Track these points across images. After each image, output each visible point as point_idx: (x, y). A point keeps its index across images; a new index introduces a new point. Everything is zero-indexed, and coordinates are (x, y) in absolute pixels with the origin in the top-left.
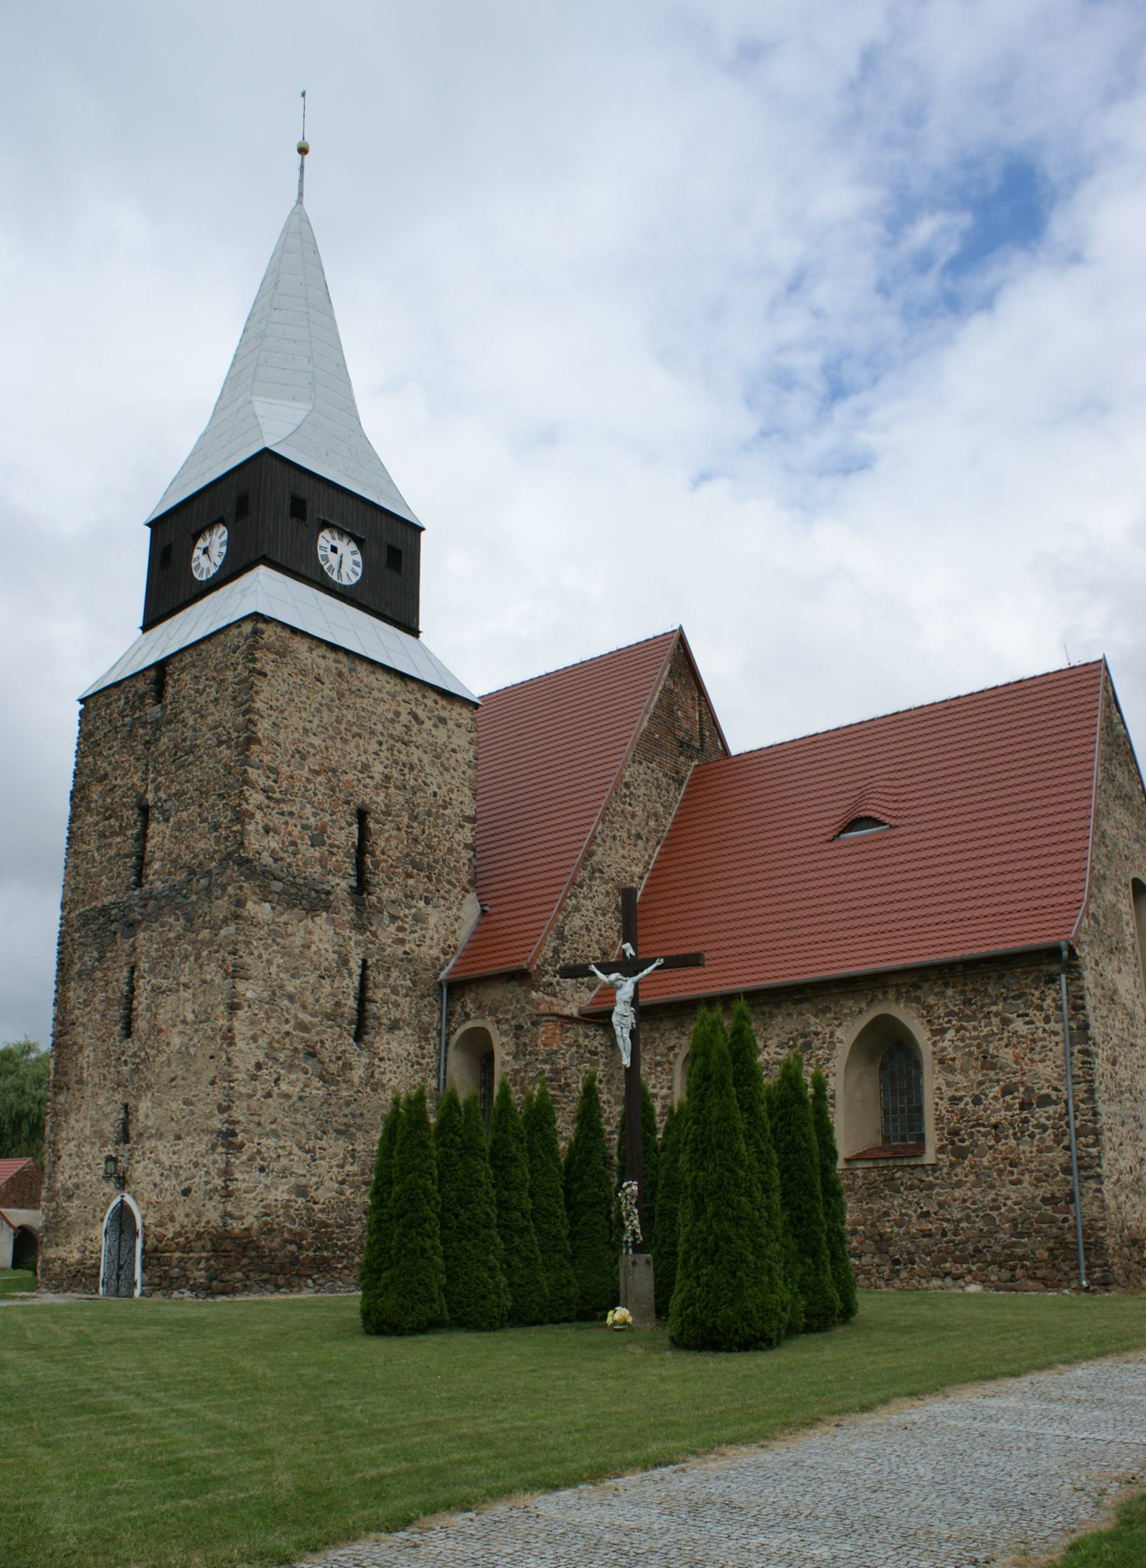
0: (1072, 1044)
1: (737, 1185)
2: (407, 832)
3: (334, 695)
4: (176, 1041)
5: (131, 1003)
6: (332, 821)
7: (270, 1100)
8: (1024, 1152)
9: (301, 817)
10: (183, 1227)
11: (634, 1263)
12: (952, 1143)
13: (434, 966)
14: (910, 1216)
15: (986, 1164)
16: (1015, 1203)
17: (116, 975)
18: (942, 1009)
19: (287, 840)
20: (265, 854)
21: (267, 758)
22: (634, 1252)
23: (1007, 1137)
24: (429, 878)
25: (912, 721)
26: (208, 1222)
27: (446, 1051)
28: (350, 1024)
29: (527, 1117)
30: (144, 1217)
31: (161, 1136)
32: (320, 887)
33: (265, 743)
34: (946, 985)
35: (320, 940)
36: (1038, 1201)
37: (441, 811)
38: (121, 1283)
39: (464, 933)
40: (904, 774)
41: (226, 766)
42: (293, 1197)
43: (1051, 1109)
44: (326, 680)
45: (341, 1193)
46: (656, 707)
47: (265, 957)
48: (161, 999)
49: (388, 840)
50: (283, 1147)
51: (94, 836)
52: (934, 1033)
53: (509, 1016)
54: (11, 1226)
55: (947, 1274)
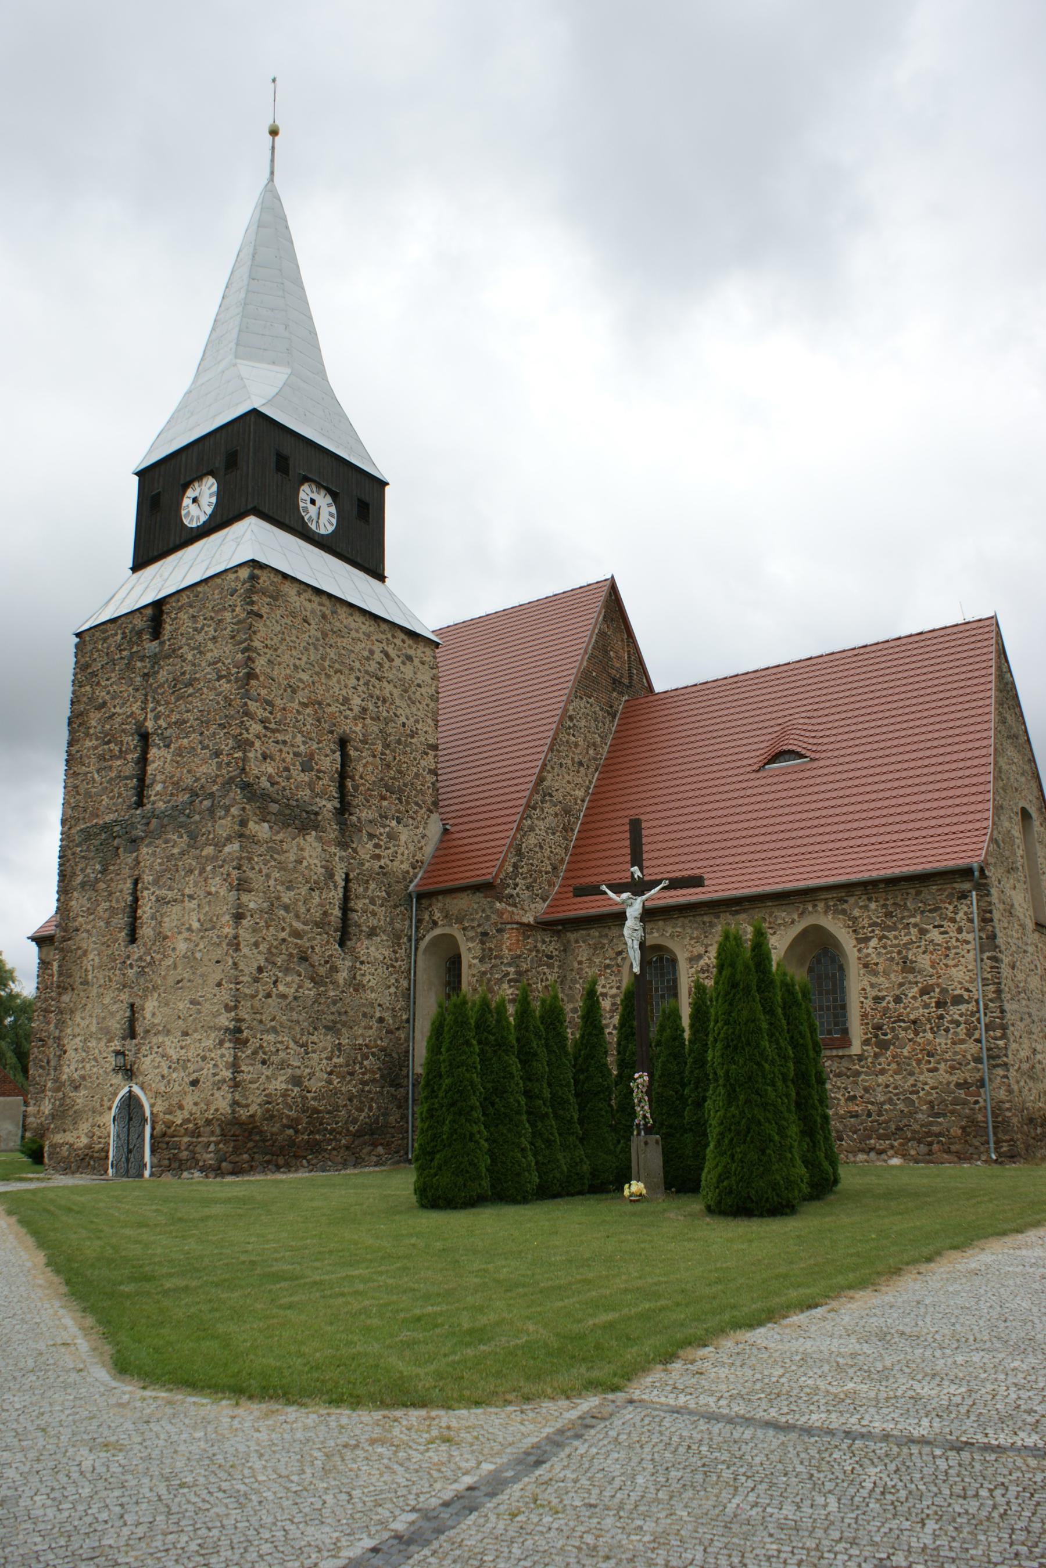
0: (982, 952)
1: (764, 1077)
3: (319, 635)
4: (182, 947)
5: (135, 912)
6: (319, 749)
7: (270, 1000)
8: (940, 1044)
9: (293, 746)
10: (191, 1114)
11: (646, 1143)
12: (876, 1036)
13: (404, 878)
14: (839, 1100)
15: (906, 1054)
16: (932, 1088)
17: (120, 887)
18: (866, 921)
19: (282, 766)
20: (264, 779)
21: (263, 692)
22: (646, 1134)
23: (925, 1031)
25: (825, 666)
26: (217, 1110)
27: (416, 955)
28: (336, 931)
29: (542, 1017)
30: (152, 1106)
31: (168, 1032)
33: (262, 679)
34: (870, 899)
35: (311, 856)
36: (952, 1086)
37: (409, 740)
38: (130, 1165)
39: (429, 850)
40: (820, 713)
41: (226, 698)
42: (290, 1087)
43: (963, 1007)
44: (312, 622)
45: (330, 1082)
46: (593, 648)
47: (265, 871)
48: (165, 909)
49: (365, 766)
50: (282, 1042)
51: (94, 760)
52: (859, 941)
53: (475, 924)
55: (872, 1149)
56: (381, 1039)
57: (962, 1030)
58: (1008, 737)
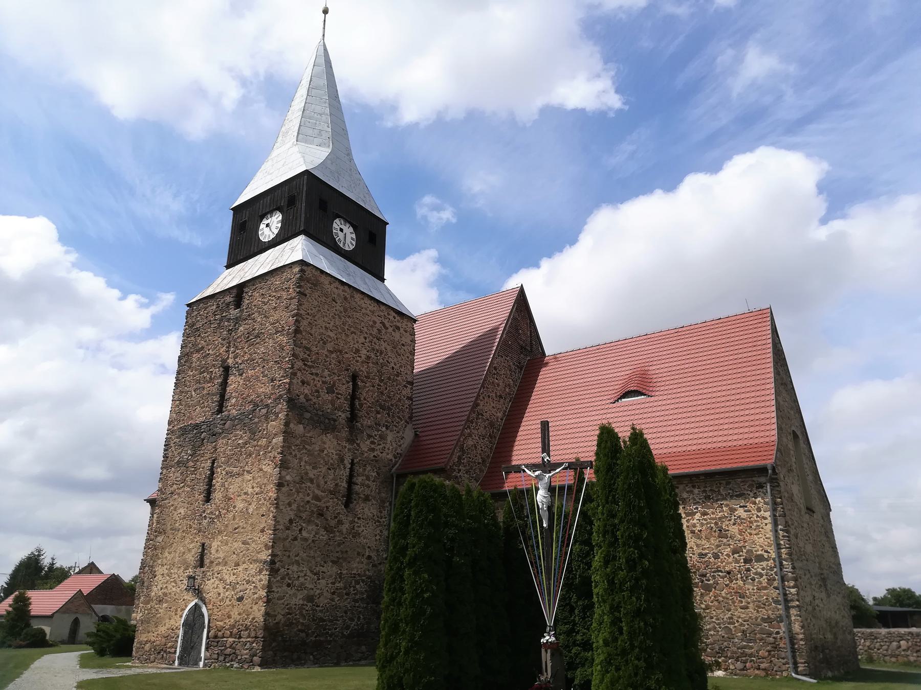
2: (378, 389)
3: (342, 309)
4: (240, 505)
6: (339, 380)
9: (322, 377)
12: (702, 582)
20: (302, 397)
23: (737, 579)
24: (388, 414)
26: (253, 619)
28: (343, 497)
31: (226, 564)
32: (331, 416)
34: (694, 487)
42: (305, 602)
43: (764, 564)
44: (338, 301)
45: (333, 600)
46: (510, 327)
50: (302, 571)
54: (97, 616)
56: (369, 570)
57: (764, 580)
58: (782, 384)
